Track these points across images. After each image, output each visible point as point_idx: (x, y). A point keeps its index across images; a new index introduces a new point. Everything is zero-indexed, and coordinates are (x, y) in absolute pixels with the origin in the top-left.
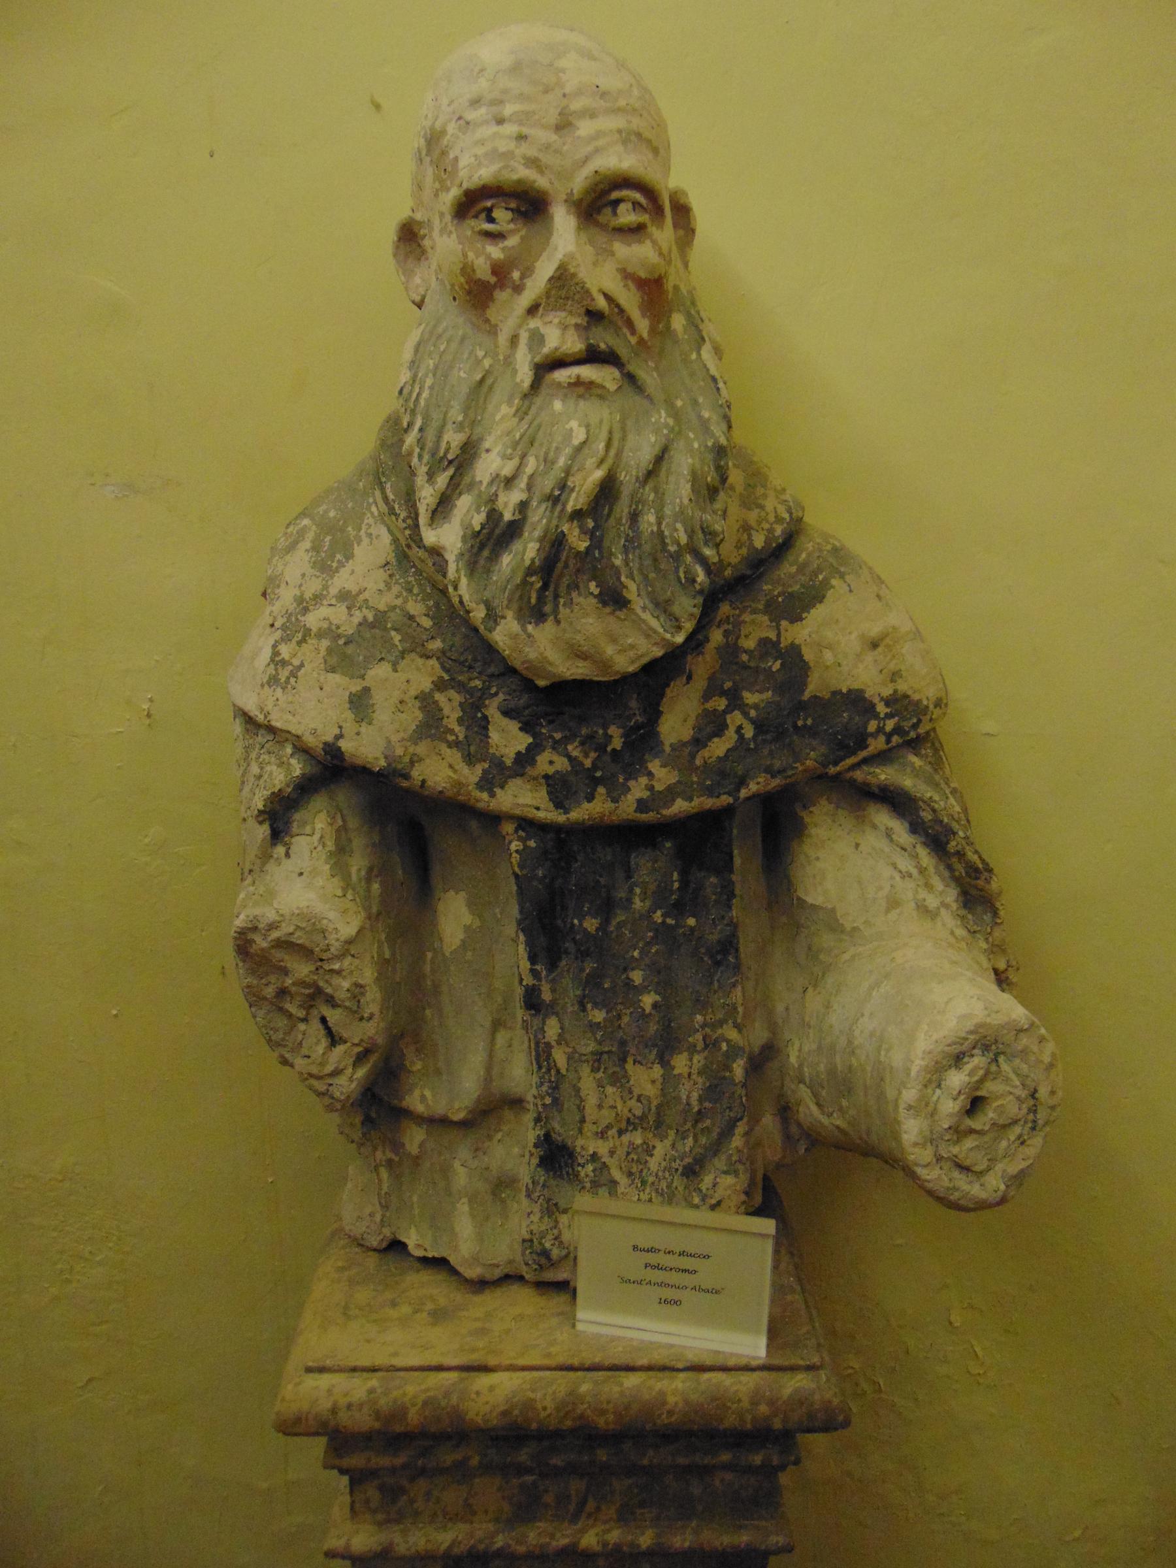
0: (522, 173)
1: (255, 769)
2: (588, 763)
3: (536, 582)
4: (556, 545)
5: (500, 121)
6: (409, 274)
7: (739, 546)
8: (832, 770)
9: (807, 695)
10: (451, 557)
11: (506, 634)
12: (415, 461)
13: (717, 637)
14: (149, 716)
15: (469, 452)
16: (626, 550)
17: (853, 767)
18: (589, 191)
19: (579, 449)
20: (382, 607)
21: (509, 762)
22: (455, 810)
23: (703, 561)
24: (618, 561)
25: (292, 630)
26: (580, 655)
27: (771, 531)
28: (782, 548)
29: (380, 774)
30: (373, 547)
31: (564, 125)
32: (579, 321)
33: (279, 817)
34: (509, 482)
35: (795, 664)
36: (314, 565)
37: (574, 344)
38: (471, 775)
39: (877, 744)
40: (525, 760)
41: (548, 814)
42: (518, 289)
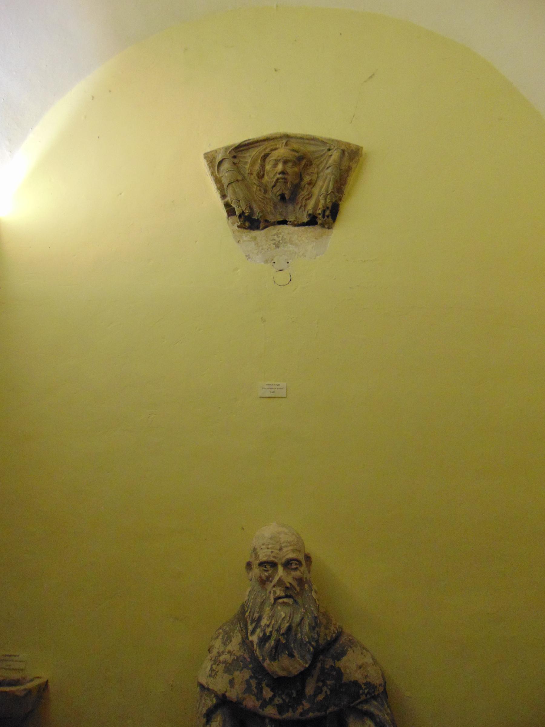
0: (272, 559)
1: (203, 701)
2: (287, 700)
3: (274, 651)
4: (278, 641)
5: (268, 549)
6: (248, 573)
7: (324, 639)
8: (352, 705)
9: (343, 682)
10: (255, 644)
11: (266, 664)
12: (248, 620)
13: (319, 665)
14: (172, 686)
15: (260, 618)
16: (294, 643)
17: (357, 705)
18: (285, 562)
19: (283, 619)
20: (238, 655)
21: (267, 700)
22: (254, 715)
23: (312, 646)
24: (292, 645)
25: (216, 661)
26: (284, 669)
27: (332, 636)
28: (336, 640)
29: (235, 703)
30: (237, 639)
31: (281, 549)
32: (240, 696)
33: (209, 716)
34: (268, 626)
35: (339, 673)
36: (222, 643)
37: (283, 594)
38: (258, 704)
39: (363, 697)
40: (272, 699)
41: (278, 716)
42: (271, 582)
